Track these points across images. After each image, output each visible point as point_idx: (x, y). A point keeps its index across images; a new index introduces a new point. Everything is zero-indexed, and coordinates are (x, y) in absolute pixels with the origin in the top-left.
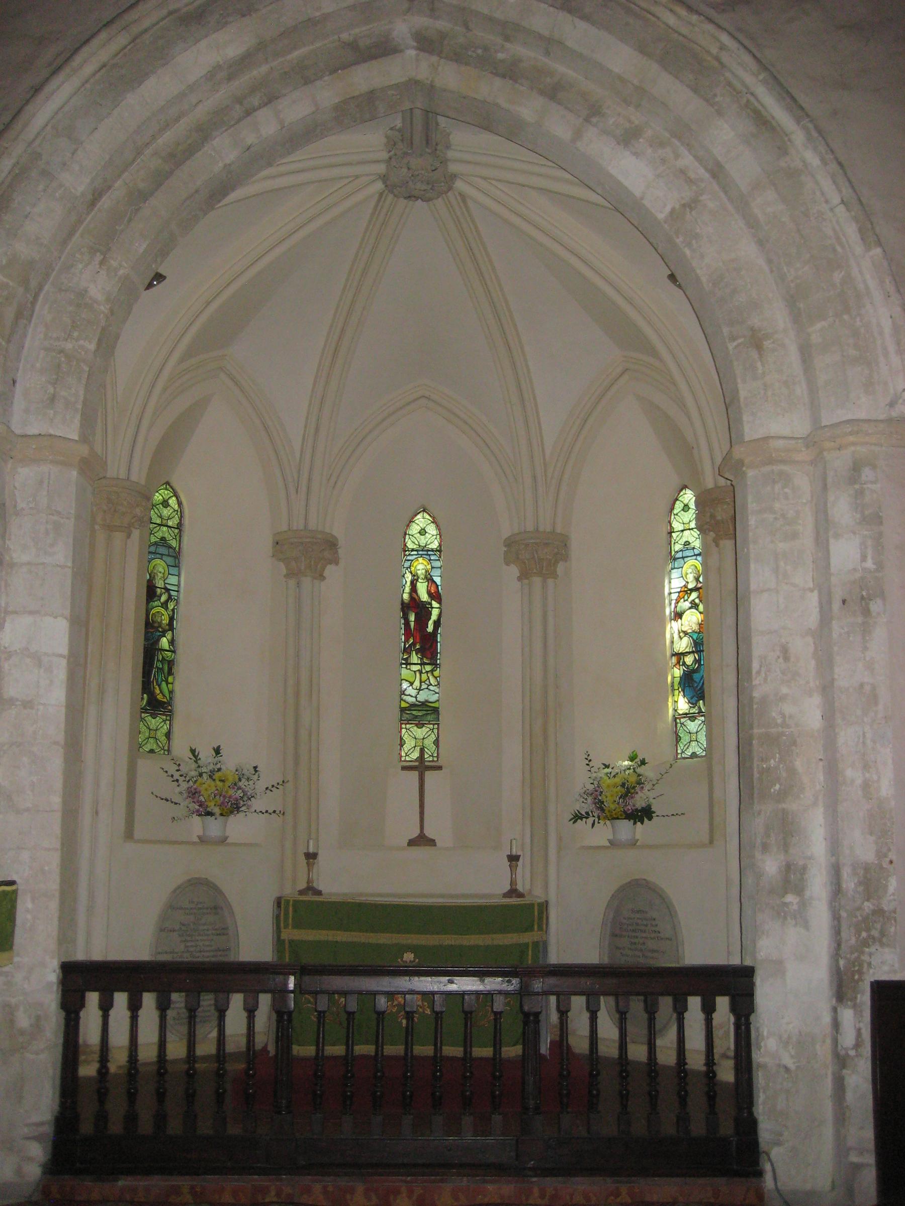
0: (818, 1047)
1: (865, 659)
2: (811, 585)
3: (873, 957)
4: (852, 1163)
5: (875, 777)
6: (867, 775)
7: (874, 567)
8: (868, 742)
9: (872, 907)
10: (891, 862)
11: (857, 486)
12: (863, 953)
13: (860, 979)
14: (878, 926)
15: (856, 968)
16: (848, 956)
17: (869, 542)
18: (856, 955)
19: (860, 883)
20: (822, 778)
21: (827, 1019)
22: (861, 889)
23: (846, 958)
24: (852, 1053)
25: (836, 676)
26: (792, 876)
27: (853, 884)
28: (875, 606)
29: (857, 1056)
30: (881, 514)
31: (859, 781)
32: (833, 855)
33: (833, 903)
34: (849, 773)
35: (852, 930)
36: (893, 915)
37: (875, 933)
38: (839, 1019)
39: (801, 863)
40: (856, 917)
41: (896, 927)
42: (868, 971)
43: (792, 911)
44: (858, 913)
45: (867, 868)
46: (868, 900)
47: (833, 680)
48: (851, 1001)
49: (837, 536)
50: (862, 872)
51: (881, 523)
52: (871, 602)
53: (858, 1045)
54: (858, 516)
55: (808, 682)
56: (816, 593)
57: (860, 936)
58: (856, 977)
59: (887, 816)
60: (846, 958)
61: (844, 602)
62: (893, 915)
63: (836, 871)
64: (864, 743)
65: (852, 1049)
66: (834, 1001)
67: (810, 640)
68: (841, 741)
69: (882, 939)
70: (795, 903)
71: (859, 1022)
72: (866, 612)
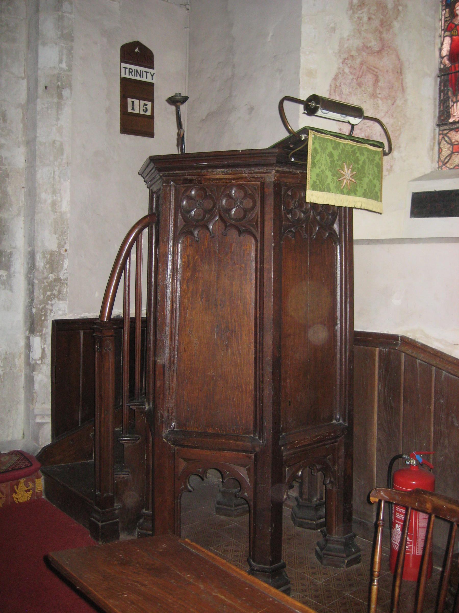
0: (16, 360)
1: (57, 125)
2: (23, 75)
3: (53, 306)
4: (38, 423)
5: (59, 199)
6: (55, 198)
7: (67, 68)
8: (57, 177)
9: (54, 277)
10: (66, 250)
11: (60, 13)
12: (48, 304)
13: (45, 320)
14: (57, 288)
15: (43, 313)
16: (38, 306)
17: (65, 52)
18: (43, 305)
19: (47, 263)
20: (23, 199)
21: (22, 343)
22: (47, 266)
23: (37, 308)
24: (39, 362)
25: (38, 135)
26: (3, 259)
27: (43, 263)
28: (66, 93)
29: (42, 363)
30: (73, 35)
31: (49, 201)
32: (29, 246)
33: (29, 276)
34: (43, 196)
35: (42, 291)
36: (66, 281)
37: (55, 292)
38: (31, 342)
39: (9, 251)
40: (44, 283)
41: (67, 288)
42: (50, 314)
43: (3, 280)
44: (45, 281)
45: (52, 254)
46: (52, 273)
47: (36, 137)
48: (39, 332)
49: (44, 44)
50: (49, 256)
51: (72, 41)
52: (63, 90)
53: (43, 357)
54: (59, 33)
55: (18, 138)
56: (25, 81)
57: (46, 294)
58: (43, 318)
59: (65, 223)
60: (37, 308)
61: (46, 87)
62: (66, 281)
63: (32, 256)
64: (54, 178)
65: (39, 360)
66: (28, 333)
67: (20, 111)
68: (39, 176)
69: (59, 296)
70: (4, 275)
71: (44, 344)
72: (60, 96)
